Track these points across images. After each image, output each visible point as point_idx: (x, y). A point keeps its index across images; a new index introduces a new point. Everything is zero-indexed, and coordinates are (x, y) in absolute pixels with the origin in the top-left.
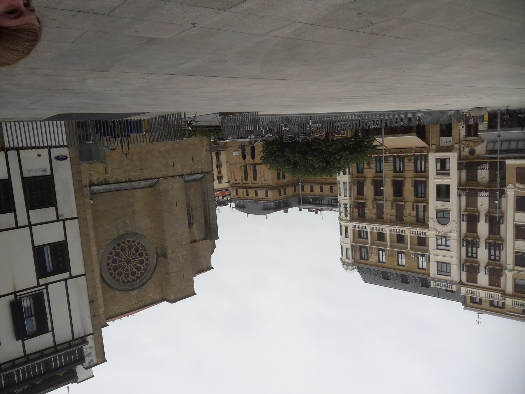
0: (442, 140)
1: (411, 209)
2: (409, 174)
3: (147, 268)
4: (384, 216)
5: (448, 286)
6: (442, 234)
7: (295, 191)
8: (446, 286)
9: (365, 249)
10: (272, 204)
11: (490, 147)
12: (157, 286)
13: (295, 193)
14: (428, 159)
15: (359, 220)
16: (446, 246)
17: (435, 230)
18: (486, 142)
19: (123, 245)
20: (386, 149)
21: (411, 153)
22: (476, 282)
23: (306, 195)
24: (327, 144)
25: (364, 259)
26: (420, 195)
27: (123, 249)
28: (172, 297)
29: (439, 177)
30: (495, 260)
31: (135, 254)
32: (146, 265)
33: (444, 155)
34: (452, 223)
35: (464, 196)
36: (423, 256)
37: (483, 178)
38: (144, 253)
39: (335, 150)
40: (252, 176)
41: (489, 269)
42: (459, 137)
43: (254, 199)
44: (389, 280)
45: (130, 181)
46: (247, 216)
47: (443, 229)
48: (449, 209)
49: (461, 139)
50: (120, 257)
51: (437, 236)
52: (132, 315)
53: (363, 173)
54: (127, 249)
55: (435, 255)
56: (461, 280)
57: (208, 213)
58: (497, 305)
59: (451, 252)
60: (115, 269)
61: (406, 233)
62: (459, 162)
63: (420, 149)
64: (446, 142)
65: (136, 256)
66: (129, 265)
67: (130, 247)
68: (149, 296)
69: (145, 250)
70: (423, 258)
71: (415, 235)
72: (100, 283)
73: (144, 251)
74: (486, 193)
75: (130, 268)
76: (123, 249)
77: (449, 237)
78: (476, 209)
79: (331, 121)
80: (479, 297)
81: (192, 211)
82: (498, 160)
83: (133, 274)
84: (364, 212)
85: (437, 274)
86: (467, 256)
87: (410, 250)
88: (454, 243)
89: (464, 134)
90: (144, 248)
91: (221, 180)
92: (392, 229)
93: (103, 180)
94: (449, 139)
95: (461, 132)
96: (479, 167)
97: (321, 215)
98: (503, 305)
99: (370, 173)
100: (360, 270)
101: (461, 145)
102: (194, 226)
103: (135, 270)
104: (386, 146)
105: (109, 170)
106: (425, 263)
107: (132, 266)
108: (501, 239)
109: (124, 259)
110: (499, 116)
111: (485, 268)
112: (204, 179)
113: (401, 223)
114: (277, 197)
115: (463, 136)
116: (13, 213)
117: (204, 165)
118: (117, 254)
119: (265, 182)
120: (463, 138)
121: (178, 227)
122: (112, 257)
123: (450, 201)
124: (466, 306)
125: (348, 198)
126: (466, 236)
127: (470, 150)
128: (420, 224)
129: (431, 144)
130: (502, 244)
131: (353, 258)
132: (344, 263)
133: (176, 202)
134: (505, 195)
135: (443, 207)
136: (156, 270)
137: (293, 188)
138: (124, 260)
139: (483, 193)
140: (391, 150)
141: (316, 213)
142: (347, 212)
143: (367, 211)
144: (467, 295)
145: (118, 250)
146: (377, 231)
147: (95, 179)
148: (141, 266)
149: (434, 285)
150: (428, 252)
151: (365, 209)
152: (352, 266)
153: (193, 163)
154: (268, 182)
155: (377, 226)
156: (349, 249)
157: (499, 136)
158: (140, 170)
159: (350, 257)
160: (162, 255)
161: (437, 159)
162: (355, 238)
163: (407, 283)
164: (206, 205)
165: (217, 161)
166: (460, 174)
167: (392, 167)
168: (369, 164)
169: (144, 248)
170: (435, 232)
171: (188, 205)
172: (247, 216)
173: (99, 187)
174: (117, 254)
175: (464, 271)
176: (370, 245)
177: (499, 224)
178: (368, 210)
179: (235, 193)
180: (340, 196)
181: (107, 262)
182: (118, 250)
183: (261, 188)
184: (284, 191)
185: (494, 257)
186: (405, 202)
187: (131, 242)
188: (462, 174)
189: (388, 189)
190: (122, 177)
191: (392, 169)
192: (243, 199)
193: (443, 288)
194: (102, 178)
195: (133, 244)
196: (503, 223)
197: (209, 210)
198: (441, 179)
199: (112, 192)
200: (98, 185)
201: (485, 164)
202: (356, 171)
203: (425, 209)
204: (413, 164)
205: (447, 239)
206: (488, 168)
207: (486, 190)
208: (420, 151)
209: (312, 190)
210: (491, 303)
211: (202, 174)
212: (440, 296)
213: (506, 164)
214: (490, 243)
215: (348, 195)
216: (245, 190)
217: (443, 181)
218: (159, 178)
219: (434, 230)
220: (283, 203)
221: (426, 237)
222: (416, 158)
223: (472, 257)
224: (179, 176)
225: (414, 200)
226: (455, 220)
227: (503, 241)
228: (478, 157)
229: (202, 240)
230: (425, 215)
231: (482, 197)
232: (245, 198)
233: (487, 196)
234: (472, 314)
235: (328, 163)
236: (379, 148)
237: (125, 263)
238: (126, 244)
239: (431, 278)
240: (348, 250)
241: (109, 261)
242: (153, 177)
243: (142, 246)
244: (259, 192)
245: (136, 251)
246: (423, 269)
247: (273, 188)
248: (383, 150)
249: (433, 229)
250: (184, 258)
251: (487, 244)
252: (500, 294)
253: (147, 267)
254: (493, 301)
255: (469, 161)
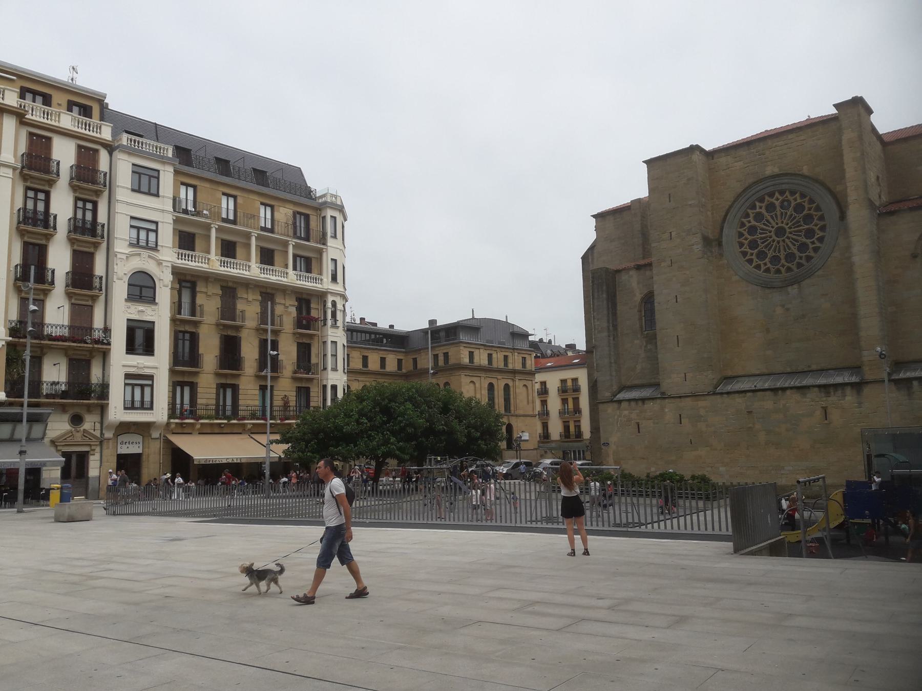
0: (139, 447)
1: (206, 308)
2: (207, 383)
3: (741, 217)
4: (260, 298)
5: (139, 144)
6: (145, 253)
7: (415, 360)
8: (142, 145)
9: (298, 235)
10: (463, 337)
11: (37, 429)
12: (722, 182)
13: (414, 357)
14: (169, 409)
15: (308, 294)
16: (138, 229)
17: (159, 263)
18: (45, 439)
19: (789, 265)
20: (252, 433)
21: (202, 424)
22: (79, 147)
23: (393, 351)
24: (387, 449)
25: (301, 214)
26: (187, 336)
27: (790, 257)
28: (696, 157)
29: (147, 372)
30: (36, 191)
31: (766, 247)
32: (743, 225)
33: (139, 416)
34: (125, 274)
35: (97, 329)
36: (186, 211)
37: (55, 365)
38: (748, 247)
39: (370, 435)
40: (496, 393)
41: (51, 170)
42: (103, 451)
43: (494, 349)
44: (253, 168)
45: (774, 390)
46: (506, 317)
47: (144, 262)
48: (129, 304)
49: (98, 449)
50: (797, 241)
51: (155, 249)
52: (812, 117)
53: (298, 387)
54: (782, 257)
55: (163, 211)
56: (111, 154)
57: (611, 322)
58: (36, 96)
59: (129, 214)
60: (808, 218)
61: (218, 260)
62: (104, 400)
63: (183, 430)
64: (130, 443)
65: (762, 243)
66: (779, 225)
67: (775, 259)
68: (741, 163)
69: (744, 254)
70: (185, 208)
71: (201, 254)
72: (848, 190)
73: (745, 251)
74: (49, 332)
75: (777, 220)
76: (790, 257)
77: (131, 245)
78: (73, 301)
79: (371, 495)
80: (72, 116)
81: (641, 327)
82: (26, 400)
83: (771, 208)
84: (299, 309)
85: (158, 171)
86: (95, 204)
87: (211, 224)
88: (122, 232)
89: (91, 458)
90: (747, 258)
91: (542, 388)
92: (246, 271)
93: (832, 393)
94: (124, 450)
95: (98, 463)
96: (63, 388)
97: (354, 315)
98: (23, 94)
99: (285, 388)
100: (308, 192)
101: (99, 435)
102: (638, 297)
103: (766, 214)
104: (252, 440)
105: (819, 413)
106: (183, 195)
107: (774, 224)
108: (21, 233)
109: (788, 238)
110: (21, 496)
111: (59, 176)
112: (615, 388)
113: (227, 281)
114: (452, 351)
115: (94, 455)
116: (137, 330)
117: (616, 417)
118: (803, 247)
119: (474, 379)
120: (94, 450)
121: (676, 296)
122: (814, 241)
123: (128, 320)
124: (100, 101)
125: (330, 339)
126: (96, 245)
127: (80, 424)
128: (188, 278)
129: (162, 440)
130: (19, 223)
131: (324, 218)
132: (341, 209)
133: (678, 346)
134: (9, 326)
135: (141, 308)
136: (724, 214)
137: (419, 366)
138: (790, 235)
139: (56, 332)
140: (241, 430)
141: (364, 319)
142: (332, 311)
143: (293, 311)
144: (100, 122)
145: (801, 255)
146: (274, 268)
147: (850, 397)
148: (753, 223)
149: (167, 149)
150: (175, 218)
151: (296, 315)
152: (325, 203)
153: (638, 421)
154: (469, 379)
155: (274, 278)
156: (332, 237)
157: (22, 453)
158: (751, 412)
159: (329, 220)
160: (712, 243)
161: (151, 408)
162: (318, 258)
163: (218, 160)
164: (614, 339)
165: (547, 422)
166: (103, 376)
167: (240, 397)
168: (286, 405)
169: (747, 258)
170: (161, 258)
171: (652, 339)
172: (506, 317)
173: (839, 380)
174: (803, 247)
175: (103, 172)
176: (289, 241)
177: (25, 266)
178: (290, 313)
179: (528, 363)
180: (343, 344)
181: (825, 232)
182: (801, 255)
183: (481, 369)
184: (438, 360)
185: (38, 198)
186: (217, 325)
187: (773, 270)
188: (100, 375)
189: (249, 351)
190: (792, 400)
191: (241, 392)
192: (514, 349)
193: (148, 141)
194: (833, 398)
195: (769, 265)
196: (16, 266)
197: (608, 327)
198: (144, 367)
199: (810, 369)
200: (843, 385)
201: (51, 394)
202: (311, 393)
203: (177, 307)
204: (199, 401)
205: (136, 243)
206: (45, 384)
207: (51, 338)
208: (184, 426)
209: (383, 360)
210: (47, 100)
211: (621, 399)
212: (154, 128)
213: (5, 392)
214: (46, 226)
215: (329, 345)
216: (510, 366)
217: (140, 362)
218: (715, 394)
219: (162, 263)
220: (440, 339)
221: (177, 250)
222: (193, 414)
223: (85, 201)
224: (670, 397)
225: (198, 327)
226: (118, 279)
227: (17, 228)
228: (63, 408)
229: (624, 269)
230: (177, 295)
231: (58, 325)
232: (511, 350)
233: (48, 327)
234: (87, 81)
235: (386, 411)
236: (278, 437)
237: (788, 230)
238: (783, 266)
239: (173, 165)
240: (333, 235)
241: (821, 234)
242: (725, 395)
243: (750, 261)
244: (485, 362)
245: (764, 251)
246: (187, 185)
247: (461, 367)
248: (268, 431)
249: (164, 264)
250: (667, 235)
251: (52, 225)
252: (29, 116)
253: (743, 220)
254: (43, 105)
255: (85, 401)
